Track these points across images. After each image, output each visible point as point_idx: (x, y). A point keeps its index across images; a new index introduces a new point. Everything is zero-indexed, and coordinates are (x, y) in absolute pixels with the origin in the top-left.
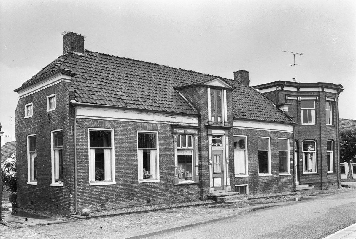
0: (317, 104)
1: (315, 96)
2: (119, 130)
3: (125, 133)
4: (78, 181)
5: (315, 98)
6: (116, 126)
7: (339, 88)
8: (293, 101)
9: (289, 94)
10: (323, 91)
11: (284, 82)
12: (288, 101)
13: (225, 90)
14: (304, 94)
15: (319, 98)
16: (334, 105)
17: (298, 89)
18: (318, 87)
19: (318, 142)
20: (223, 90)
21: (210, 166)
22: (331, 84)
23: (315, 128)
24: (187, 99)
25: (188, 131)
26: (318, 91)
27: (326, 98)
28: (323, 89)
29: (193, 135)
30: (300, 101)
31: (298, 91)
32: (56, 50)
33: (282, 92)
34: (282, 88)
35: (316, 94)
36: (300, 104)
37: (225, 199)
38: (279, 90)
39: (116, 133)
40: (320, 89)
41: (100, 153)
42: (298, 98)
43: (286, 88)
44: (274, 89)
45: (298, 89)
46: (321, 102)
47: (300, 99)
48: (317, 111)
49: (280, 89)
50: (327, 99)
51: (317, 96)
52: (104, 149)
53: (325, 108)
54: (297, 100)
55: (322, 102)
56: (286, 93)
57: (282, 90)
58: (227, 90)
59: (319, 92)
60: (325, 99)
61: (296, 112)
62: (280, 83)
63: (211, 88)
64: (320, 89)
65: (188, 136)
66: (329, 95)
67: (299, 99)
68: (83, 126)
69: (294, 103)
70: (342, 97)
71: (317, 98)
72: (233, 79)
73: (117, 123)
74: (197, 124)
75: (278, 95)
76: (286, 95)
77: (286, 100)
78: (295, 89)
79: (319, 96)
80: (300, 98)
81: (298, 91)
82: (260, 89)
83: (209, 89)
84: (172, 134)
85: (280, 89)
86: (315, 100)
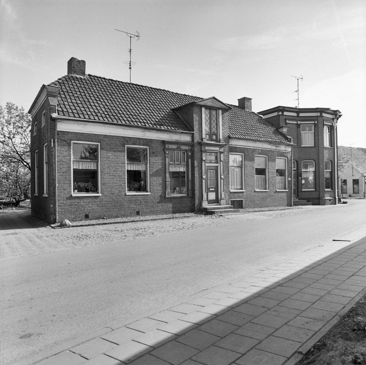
0: (316, 127)
1: (314, 120)
2: (105, 144)
3: (111, 147)
4: (59, 192)
5: (313, 122)
6: (102, 140)
7: (336, 114)
8: (293, 125)
9: (289, 118)
10: (321, 116)
11: (284, 107)
12: (288, 124)
13: (220, 110)
14: (303, 118)
15: (318, 122)
16: (332, 130)
17: (298, 114)
18: (317, 112)
19: (316, 162)
20: (219, 110)
21: (204, 181)
22: (328, 109)
23: (313, 150)
24: (183, 118)
25: (181, 147)
26: (317, 115)
27: (324, 122)
28: (321, 114)
29: (186, 151)
30: (300, 124)
31: (298, 116)
32: (62, 71)
33: (283, 117)
34: (283, 112)
35: (315, 118)
36: (300, 127)
37: (215, 211)
38: (279, 115)
39: (102, 147)
40: (319, 114)
41: (283, 175)
42: (298, 122)
43: (285, 113)
44: (276, 114)
45: (298, 114)
46: (319, 126)
47: (300, 123)
48: (316, 134)
49: (280, 113)
50: (325, 123)
51: (316, 120)
52: (97, 162)
53: (323, 131)
54: (297, 124)
55: (320, 125)
56: (287, 117)
57: (283, 115)
58: (222, 110)
59: (318, 116)
60: (324, 122)
61: (296, 135)
62: (280, 108)
63: (205, 108)
64: (319, 114)
65: (181, 152)
66: (328, 120)
67: (298, 123)
68: (65, 139)
69: (295, 127)
70: (340, 125)
71: (316, 122)
72: (237, 105)
73: (103, 138)
74: (256, 156)
75: (279, 119)
76: (286, 119)
77: (286, 124)
78: (295, 114)
79: (317, 120)
80: (300, 122)
81: (298, 116)
82: (263, 115)
83: (203, 109)
84: (164, 150)
85: (280, 113)
86: (315, 124)
